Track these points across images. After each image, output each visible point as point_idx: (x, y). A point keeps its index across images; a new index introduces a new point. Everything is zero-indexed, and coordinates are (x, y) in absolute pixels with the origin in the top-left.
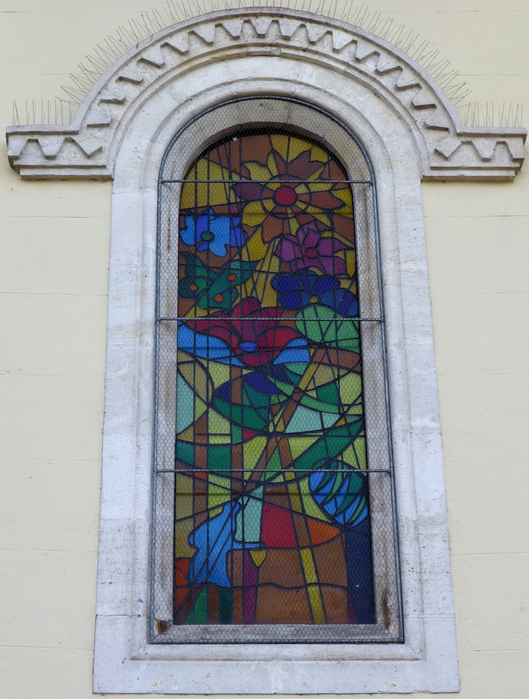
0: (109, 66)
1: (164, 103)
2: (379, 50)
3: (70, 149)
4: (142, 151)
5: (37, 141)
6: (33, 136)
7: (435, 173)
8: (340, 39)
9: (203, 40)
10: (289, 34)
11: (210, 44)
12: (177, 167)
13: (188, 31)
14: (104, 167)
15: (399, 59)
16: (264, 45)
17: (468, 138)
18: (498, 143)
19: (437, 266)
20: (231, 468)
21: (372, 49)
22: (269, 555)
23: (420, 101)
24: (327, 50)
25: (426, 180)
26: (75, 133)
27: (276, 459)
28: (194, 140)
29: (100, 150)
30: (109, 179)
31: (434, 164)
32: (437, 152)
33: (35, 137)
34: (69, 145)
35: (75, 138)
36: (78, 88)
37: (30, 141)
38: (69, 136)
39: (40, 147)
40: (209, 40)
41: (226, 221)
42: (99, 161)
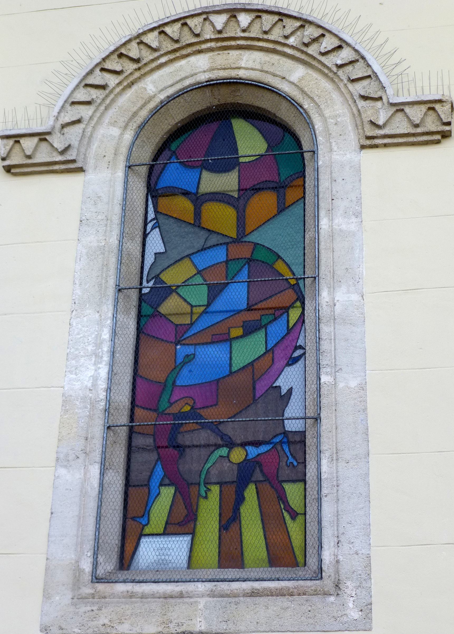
0: (83, 67)
1: (128, 100)
3: (431, 117)
4: (112, 142)
5: (403, 110)
11: (177, 41)
12: (145, 154)
13: (158, 31)
14: (74, 161)
15: (341, 39)
17: (399, 108)
18: (430, 109)
19: (377, 224)
22: (223, 489)
25: (363, 147)
26: (49, 133)
30: (81, 170)
31: (370, 134)
32: (372, 123)
33: (402, 107)
34: (431, 112)
35: (47, 137)
36: (53, 92)
37: (397, 111)
38: (42, 137)
40: (176, 38)
41: (162, 201)
42: (69, 156)
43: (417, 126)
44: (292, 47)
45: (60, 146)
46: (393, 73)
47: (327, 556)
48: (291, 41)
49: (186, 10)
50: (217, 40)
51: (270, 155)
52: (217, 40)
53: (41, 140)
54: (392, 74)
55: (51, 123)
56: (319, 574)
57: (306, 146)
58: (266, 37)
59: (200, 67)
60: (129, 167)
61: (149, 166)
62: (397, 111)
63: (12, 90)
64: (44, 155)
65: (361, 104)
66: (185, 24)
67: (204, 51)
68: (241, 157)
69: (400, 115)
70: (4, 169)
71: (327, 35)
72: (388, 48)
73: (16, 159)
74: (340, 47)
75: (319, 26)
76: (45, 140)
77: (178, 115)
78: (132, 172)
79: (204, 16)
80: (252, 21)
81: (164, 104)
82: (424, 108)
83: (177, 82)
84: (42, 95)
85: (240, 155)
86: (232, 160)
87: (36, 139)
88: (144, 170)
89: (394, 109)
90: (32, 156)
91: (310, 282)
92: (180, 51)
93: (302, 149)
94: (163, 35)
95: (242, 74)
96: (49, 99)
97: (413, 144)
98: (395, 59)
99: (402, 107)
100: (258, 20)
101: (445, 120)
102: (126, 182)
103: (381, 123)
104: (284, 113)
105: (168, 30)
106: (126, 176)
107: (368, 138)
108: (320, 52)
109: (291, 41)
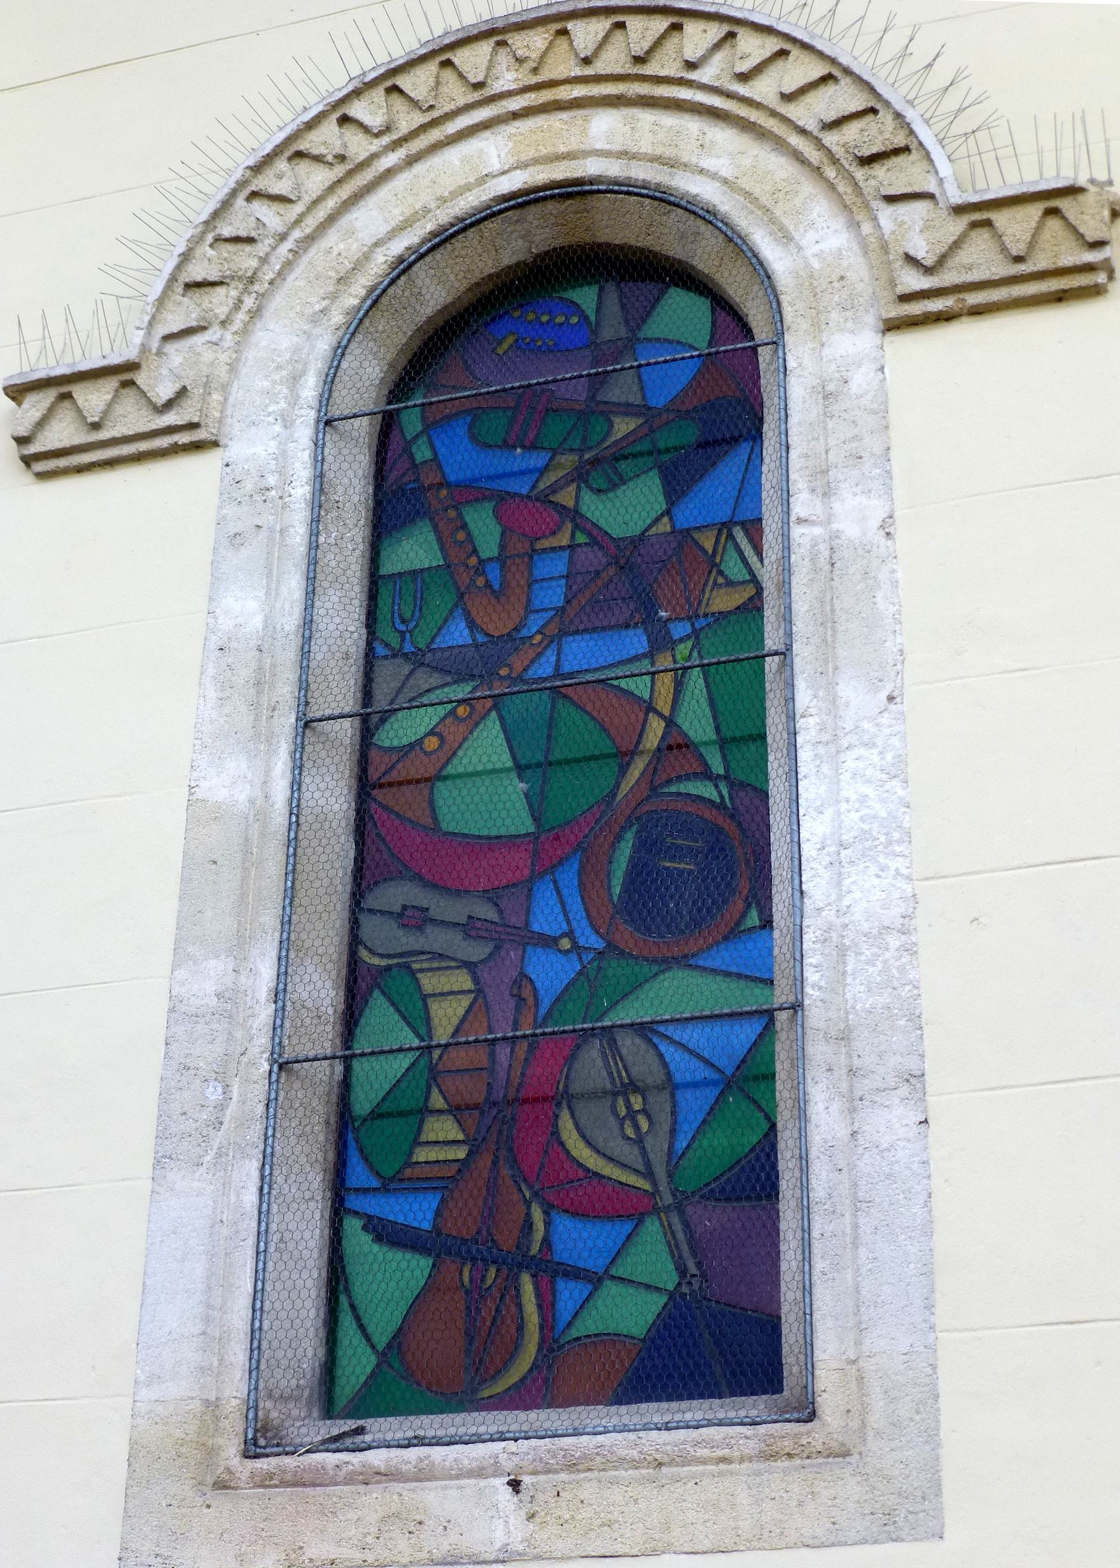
2: (787, 46)
5: (988, 223)
6: (61, 386)
7: (916, 308)
8: (697, 38)
9: (414, 103)
10: (480, 78)
14: (193, 426)
16: (599, 79)
17: (979, 214)
20: (515, 1029)
21: (773, 45)
23: (866, 145)
24: (671, 69)
25: (892, 326)
27: (444, 1022)
28: (397, 332)
29: (183, 392)
30: (215, 444)
33: (985, 215)
37: (974, 225)
38: (123, 374)
39: (998, 236)
43: (96, 426)
45: (164, 392)
46: (955, 130)
48: (704, 75)
49: (456, 26)
51: (468, 396)
54: (951, 133)
55: (138, 338)
57: (761, 333)
59: (492, 163)
60: (328, 423)
61: (380, 417)
62: (974, 225)
63: (28, 272)
64: (131, 418)
66: (448, 63)
67: (466, 132)
68: (760, 345)
69: (984, 234)
71: (795, 52)
72: (921, 53)
73: (62, 432)
75: (768, 30)
77: (434, 292)
78: (336, 437)
79: (558, 26)
80: (606, 38)
81: (403, 267)
82: (1035, 211)
84: (114, 273)
85: (758, 341)
86: (441, 406)
88: (363, 429)
89: (964, 221)
90: (96, 420)
91: (774, 667)
92: (434, 133)
94: (395, 96)
95: (591, 168)
96: (137, 285)
97: (80, 470)
99: (985, 215)
100: (618, 35)
101: (1091, 236)
102: (319, 459)
106: (318, 445)
107: (905, 298)
109: (704, 75)
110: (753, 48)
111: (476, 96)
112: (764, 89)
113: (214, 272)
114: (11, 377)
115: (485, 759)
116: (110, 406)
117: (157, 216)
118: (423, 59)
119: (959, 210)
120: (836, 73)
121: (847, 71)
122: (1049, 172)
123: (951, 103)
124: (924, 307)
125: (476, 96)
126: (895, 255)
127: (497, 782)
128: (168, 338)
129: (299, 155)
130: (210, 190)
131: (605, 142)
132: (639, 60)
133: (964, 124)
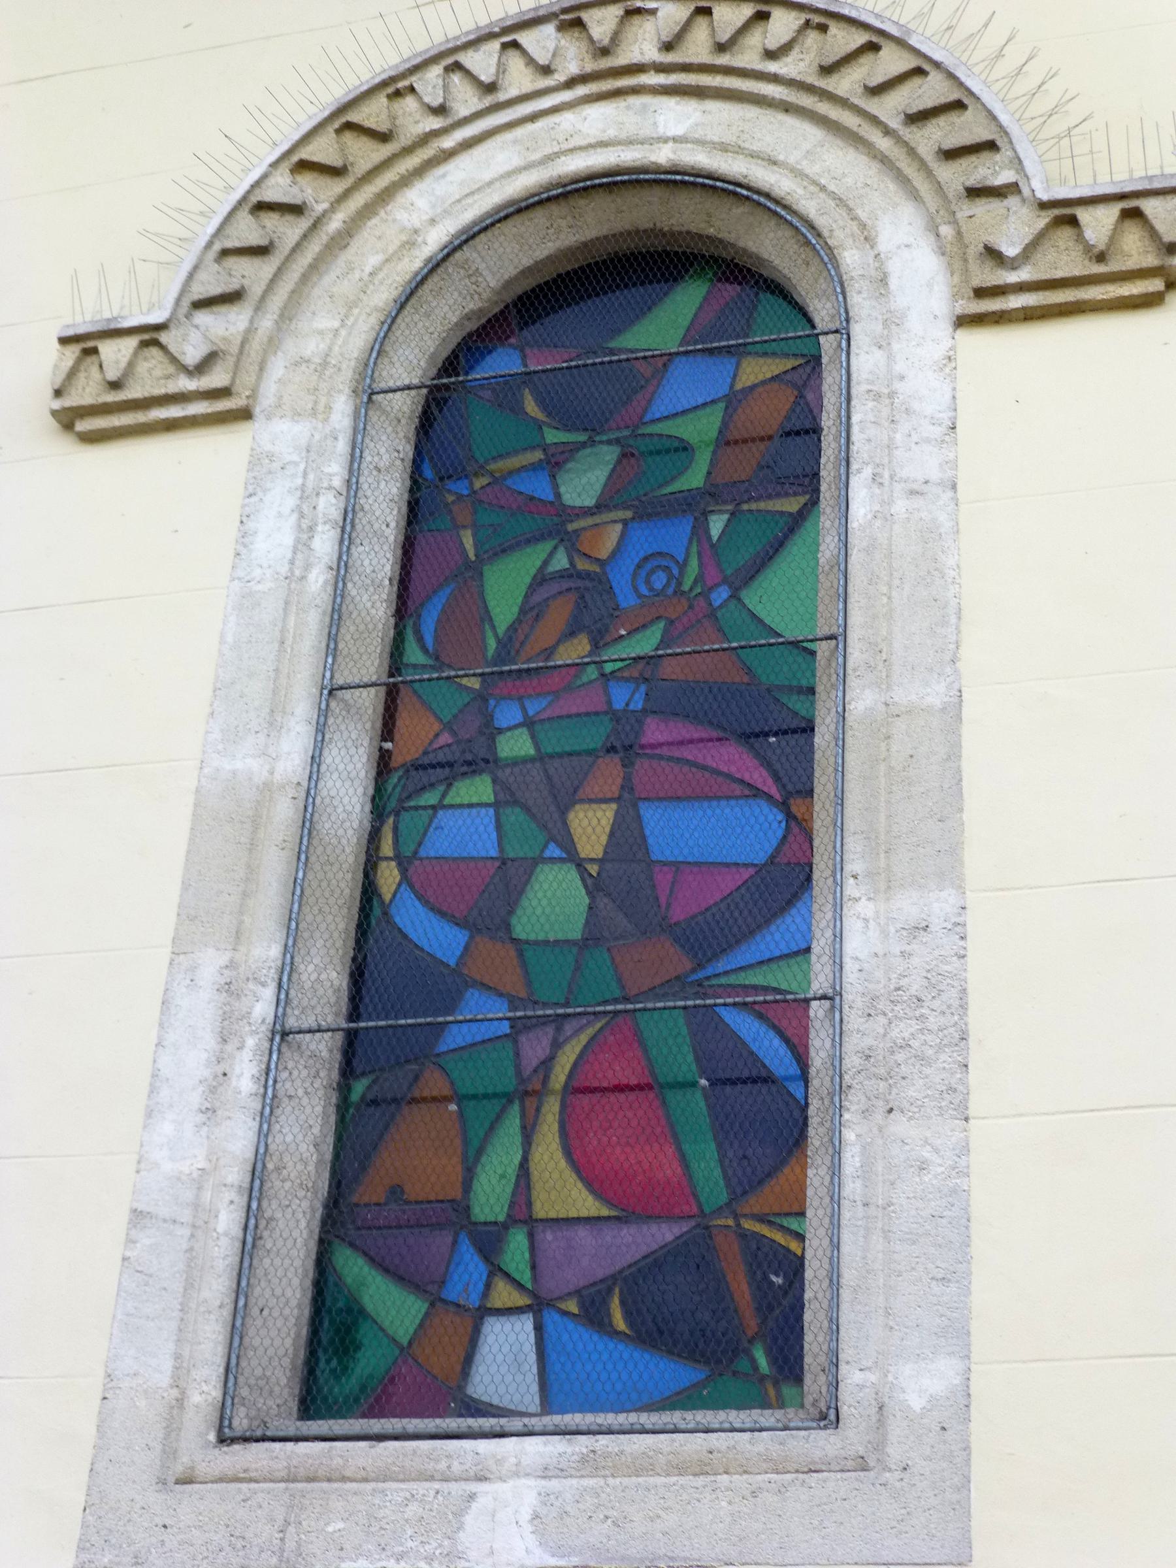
17: (1064, 215)
25: (964, 321)
30: (245, 414)
38: (150, 336)
44: (791, 83)
45: (192, 354)
47: (852, 1377)
50: (661, 68)
52: (661, 68)
53: (145, 344)
54: (1027, 115)
56: (829, 1417)
58: (724, 60)
61: (425, 391)
65: (966, 209)
70: (59, 422)
72: (1014, 56)
74: (919, 72)
76: (156, 343)
83: (630, 142)
87: (132, 342)
90: (117, 391)
93: (813, 327)
98: (1014, 56)
103: (1011, 251)
104: (768, 246)
105: (469, 59)
107: (981, 293)
108: (866, 87)
110: (843, 40)
111: (488, 101)
112: (846, 83)
113: (272, 230)
114: (56, 366)
115: (686, 851)
116: (131, 365)
117: (271, 117)
118: (491, 36)
119: (1044, 206)
120: (926, 67)
121: (937, 65)
122: (1104, 178)
123: (1040, 106)
124: (989, 304)
125: (488, 101)
126: (975, 249)
127: (783, 946)
128: (199, 305)
129: (349, 126)
130: (277, 136)
131: (671, 130)
132: (721, 48)
133: (1058, 125)
